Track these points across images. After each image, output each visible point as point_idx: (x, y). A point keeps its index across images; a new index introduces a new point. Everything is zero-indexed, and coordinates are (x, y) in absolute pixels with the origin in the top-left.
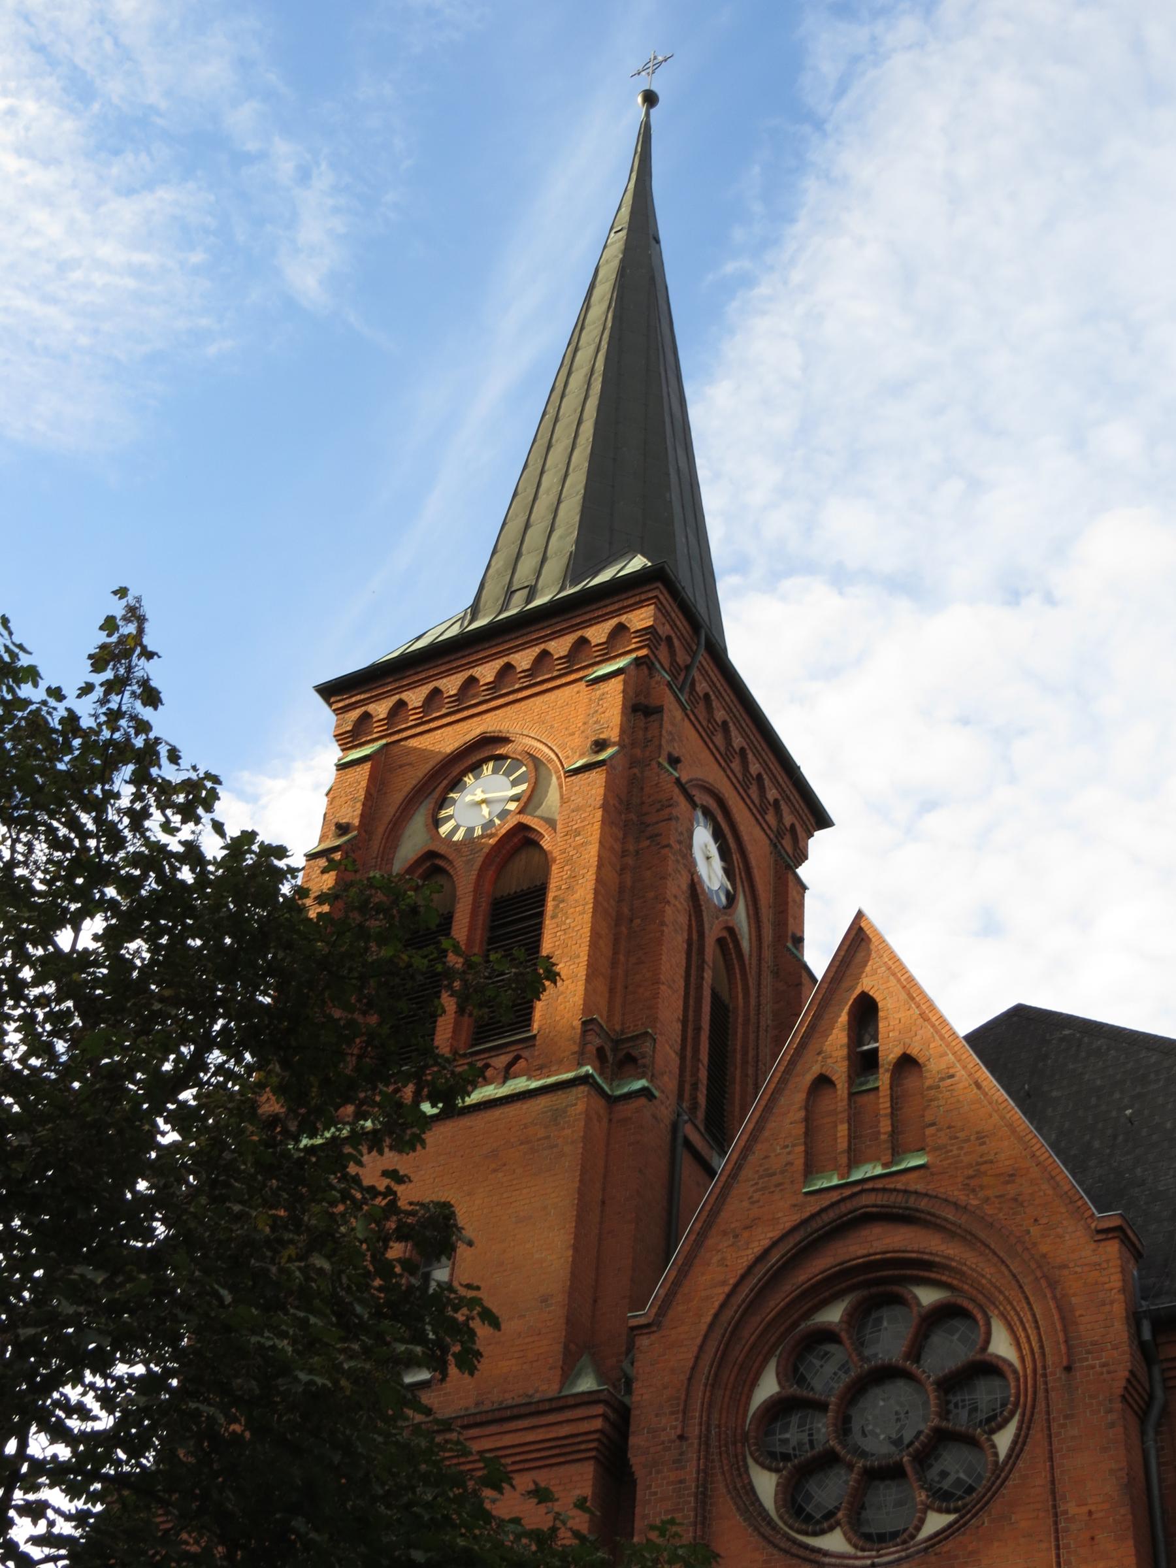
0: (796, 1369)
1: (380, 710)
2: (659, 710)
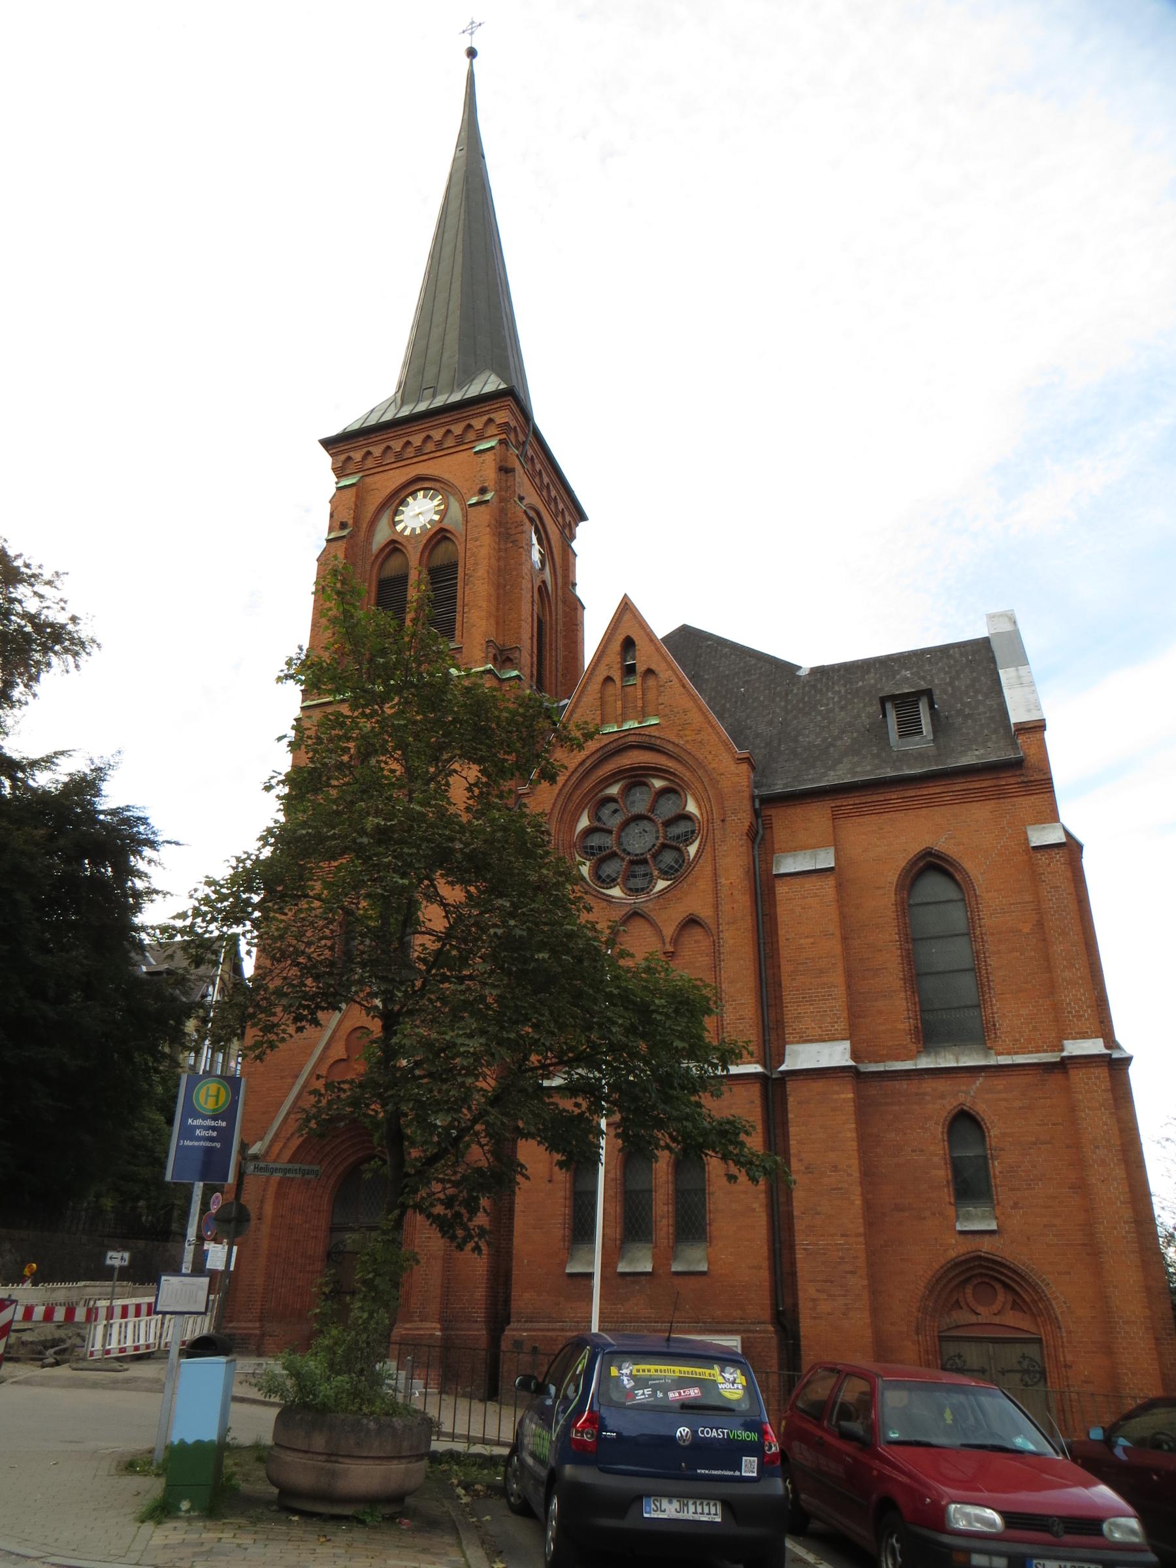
0: (597, 814)
2: (513, 470)
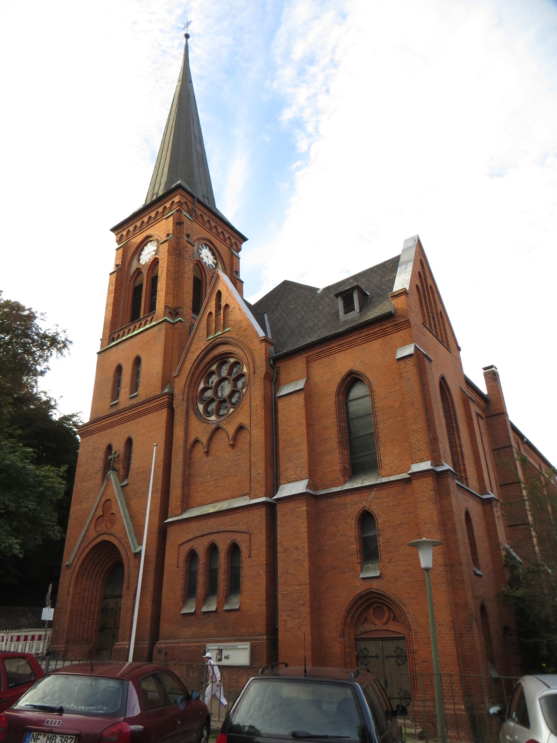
1: (124, 233)
2: (183, 223)
